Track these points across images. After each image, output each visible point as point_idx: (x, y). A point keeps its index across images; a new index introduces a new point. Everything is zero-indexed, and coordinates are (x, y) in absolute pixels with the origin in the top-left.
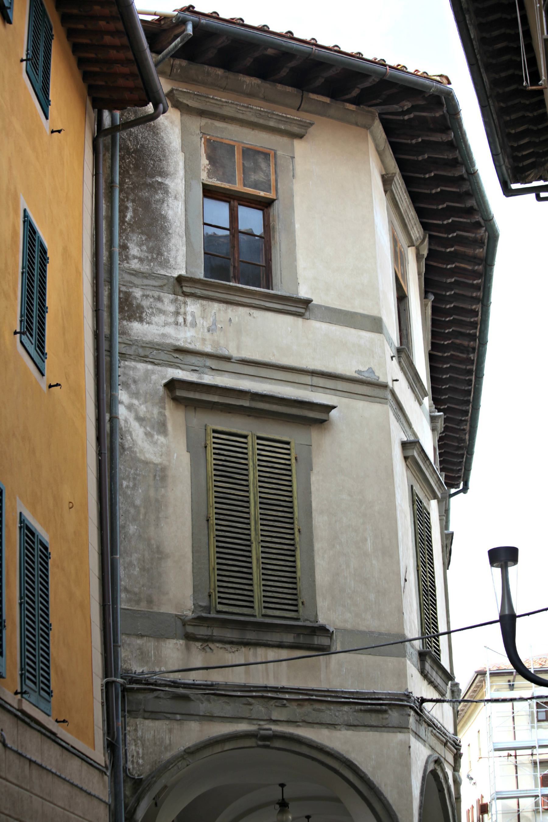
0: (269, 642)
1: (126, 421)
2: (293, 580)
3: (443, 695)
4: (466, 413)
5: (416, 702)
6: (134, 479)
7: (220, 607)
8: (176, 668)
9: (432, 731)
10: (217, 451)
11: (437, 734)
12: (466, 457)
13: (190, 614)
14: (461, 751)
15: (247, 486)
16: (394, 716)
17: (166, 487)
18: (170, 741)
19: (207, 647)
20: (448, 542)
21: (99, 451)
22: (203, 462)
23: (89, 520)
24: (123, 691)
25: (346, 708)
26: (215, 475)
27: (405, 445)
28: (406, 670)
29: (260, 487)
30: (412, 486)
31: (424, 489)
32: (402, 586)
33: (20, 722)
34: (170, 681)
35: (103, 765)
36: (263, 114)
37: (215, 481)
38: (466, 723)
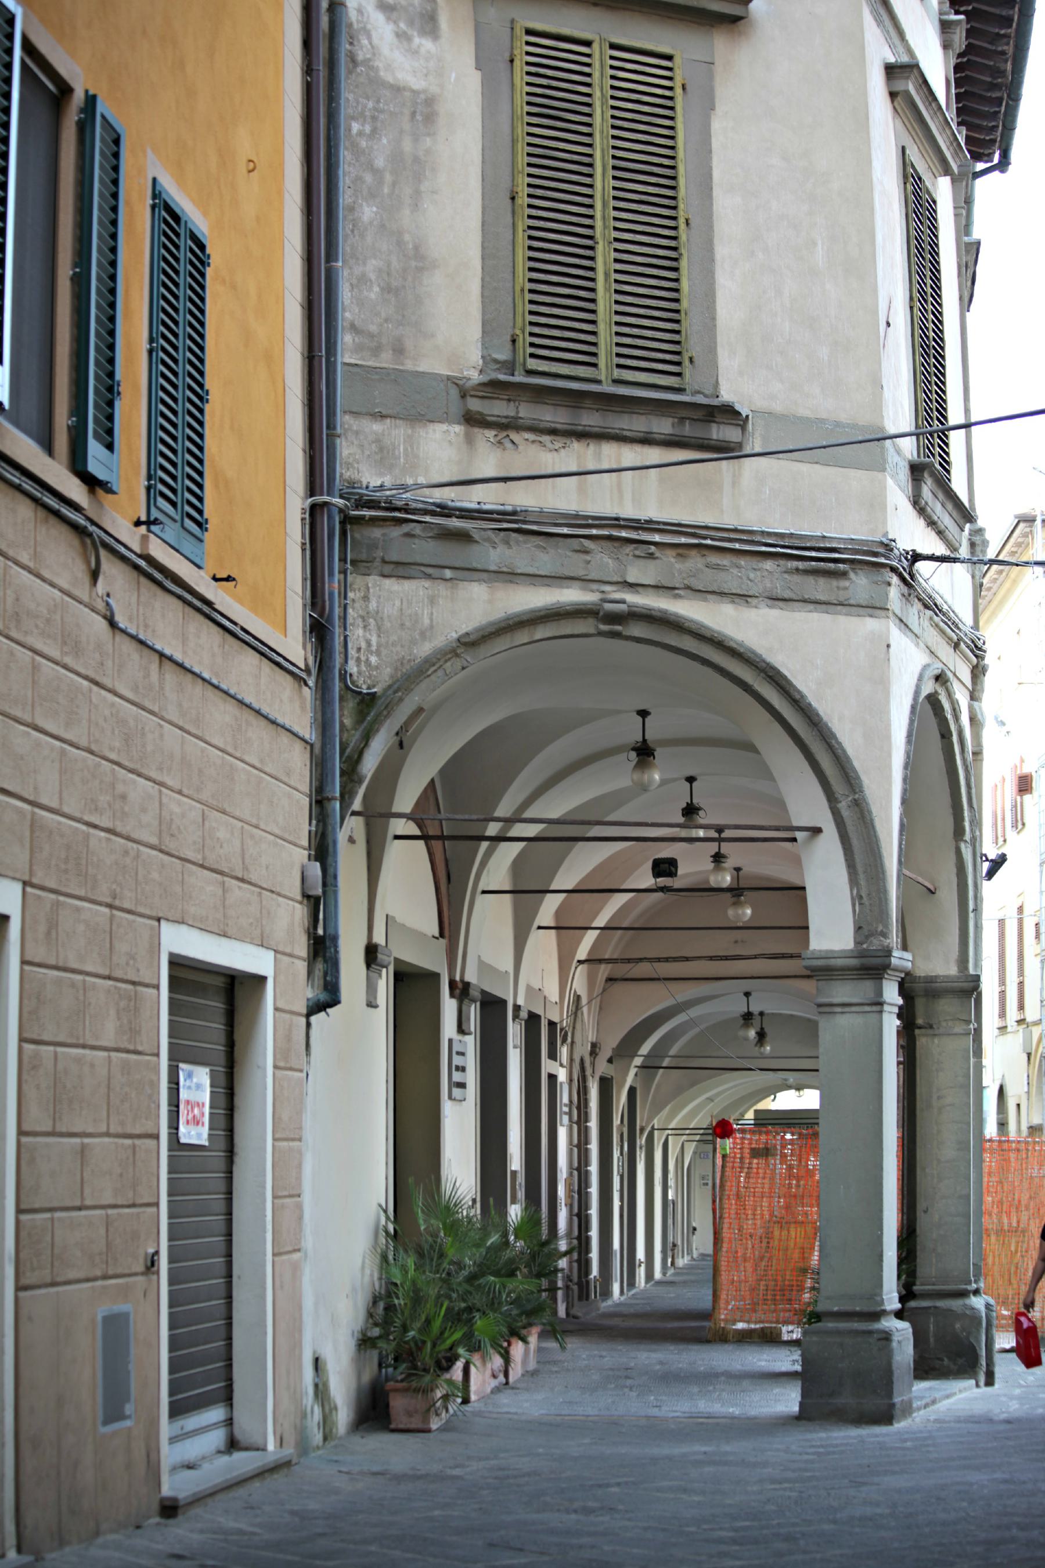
0: (625, 433)
1: (360, 11)
2: (674, 316)
3: (955, 550)
4: (1008, 21)
5: (903, 559)
6: (374, 118)
7: (533, 364)
8: (445, 479)
9: (931, 618)
10: (533, 69)
11: (942, 624)
12: (1007, 103)
13: (475, 377)
14: (986, 661)
15: (590, 135)
16: (860, 584)
17: (434, 134)
18: (431, 620)
19: (507, 440)
20: (969, 258)
21: (308, 66)
22: (505, 88)
23: (287, 195)
24: (343, 523)
25: (769, 565)
26: (528, 114)
27: (891, 70)
28: (886, 497)
29: (614, 137)
30: (903, 149)
31: (926, 155)
32: (882, 334)
33: (143, 580)
34: (434, 504)
35: (303, 667)
37: (528, 124)
38: (994, 613)
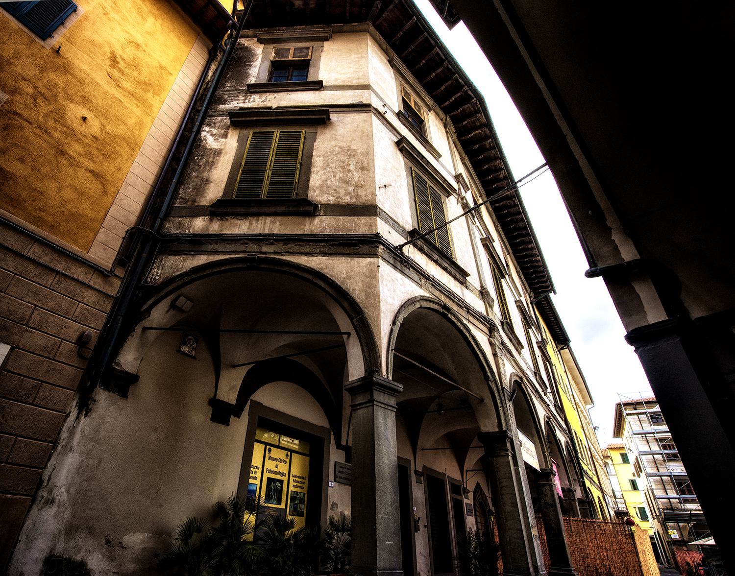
36: (303, 32)
